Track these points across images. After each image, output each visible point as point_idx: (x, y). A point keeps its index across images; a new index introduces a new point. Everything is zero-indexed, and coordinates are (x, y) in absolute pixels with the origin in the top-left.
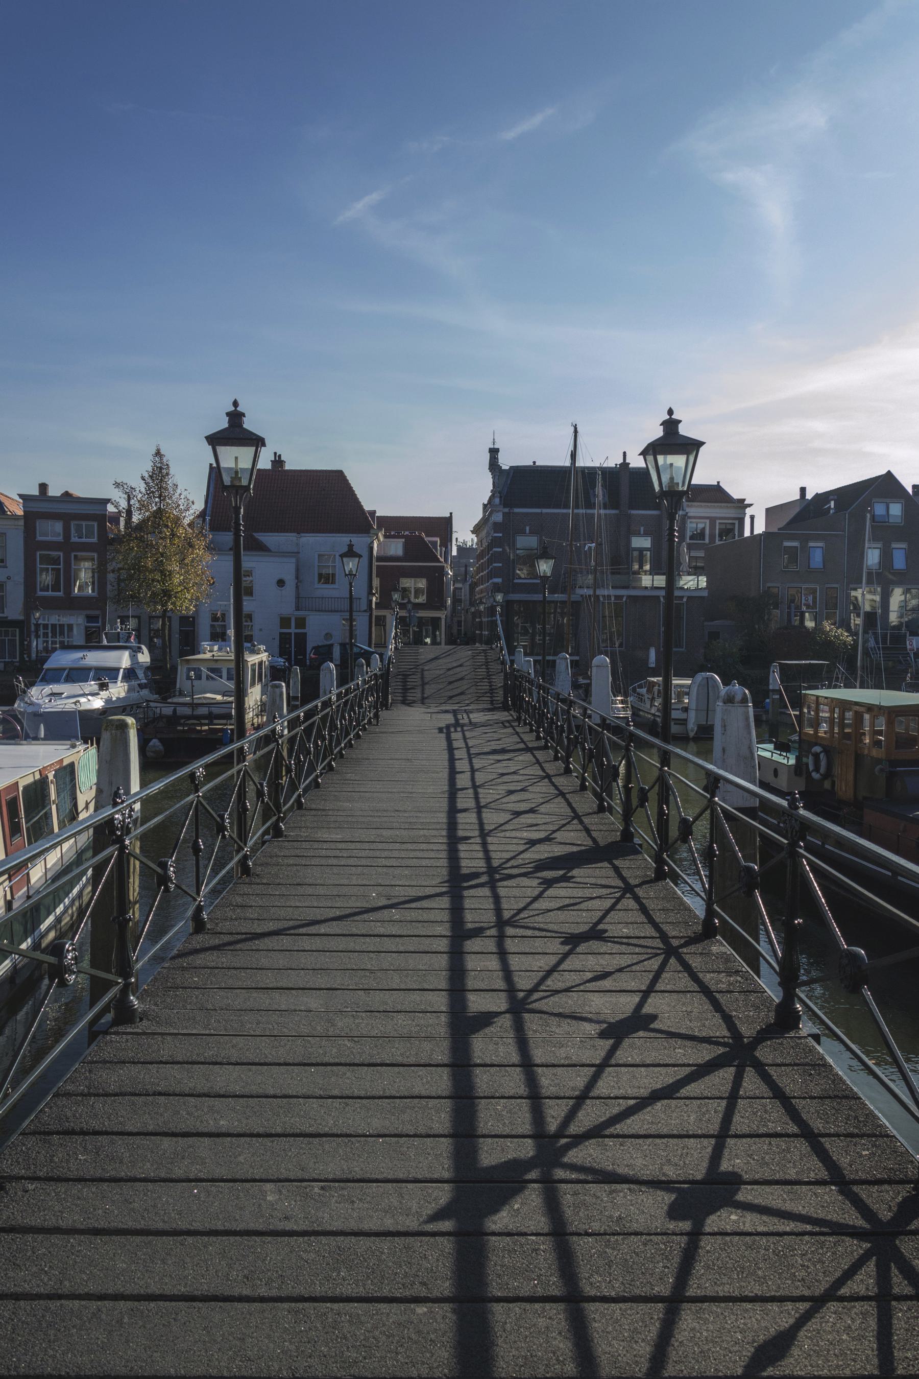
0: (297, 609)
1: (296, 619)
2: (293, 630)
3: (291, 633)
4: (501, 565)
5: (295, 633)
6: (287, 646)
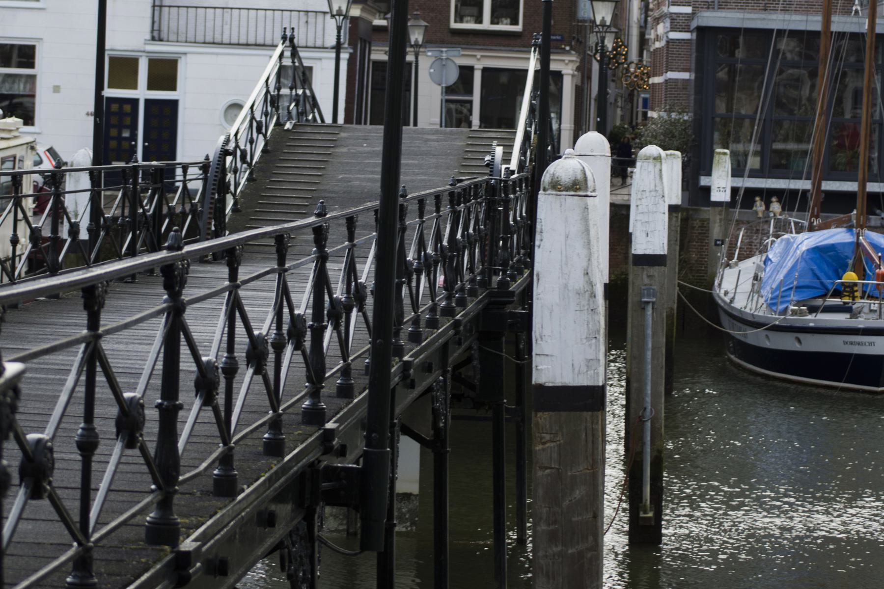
0: (157, 36)
1: (154, 64)
2: (142, 93)
3: (134, 102)
5: (148, 102)
6: (126, 134)
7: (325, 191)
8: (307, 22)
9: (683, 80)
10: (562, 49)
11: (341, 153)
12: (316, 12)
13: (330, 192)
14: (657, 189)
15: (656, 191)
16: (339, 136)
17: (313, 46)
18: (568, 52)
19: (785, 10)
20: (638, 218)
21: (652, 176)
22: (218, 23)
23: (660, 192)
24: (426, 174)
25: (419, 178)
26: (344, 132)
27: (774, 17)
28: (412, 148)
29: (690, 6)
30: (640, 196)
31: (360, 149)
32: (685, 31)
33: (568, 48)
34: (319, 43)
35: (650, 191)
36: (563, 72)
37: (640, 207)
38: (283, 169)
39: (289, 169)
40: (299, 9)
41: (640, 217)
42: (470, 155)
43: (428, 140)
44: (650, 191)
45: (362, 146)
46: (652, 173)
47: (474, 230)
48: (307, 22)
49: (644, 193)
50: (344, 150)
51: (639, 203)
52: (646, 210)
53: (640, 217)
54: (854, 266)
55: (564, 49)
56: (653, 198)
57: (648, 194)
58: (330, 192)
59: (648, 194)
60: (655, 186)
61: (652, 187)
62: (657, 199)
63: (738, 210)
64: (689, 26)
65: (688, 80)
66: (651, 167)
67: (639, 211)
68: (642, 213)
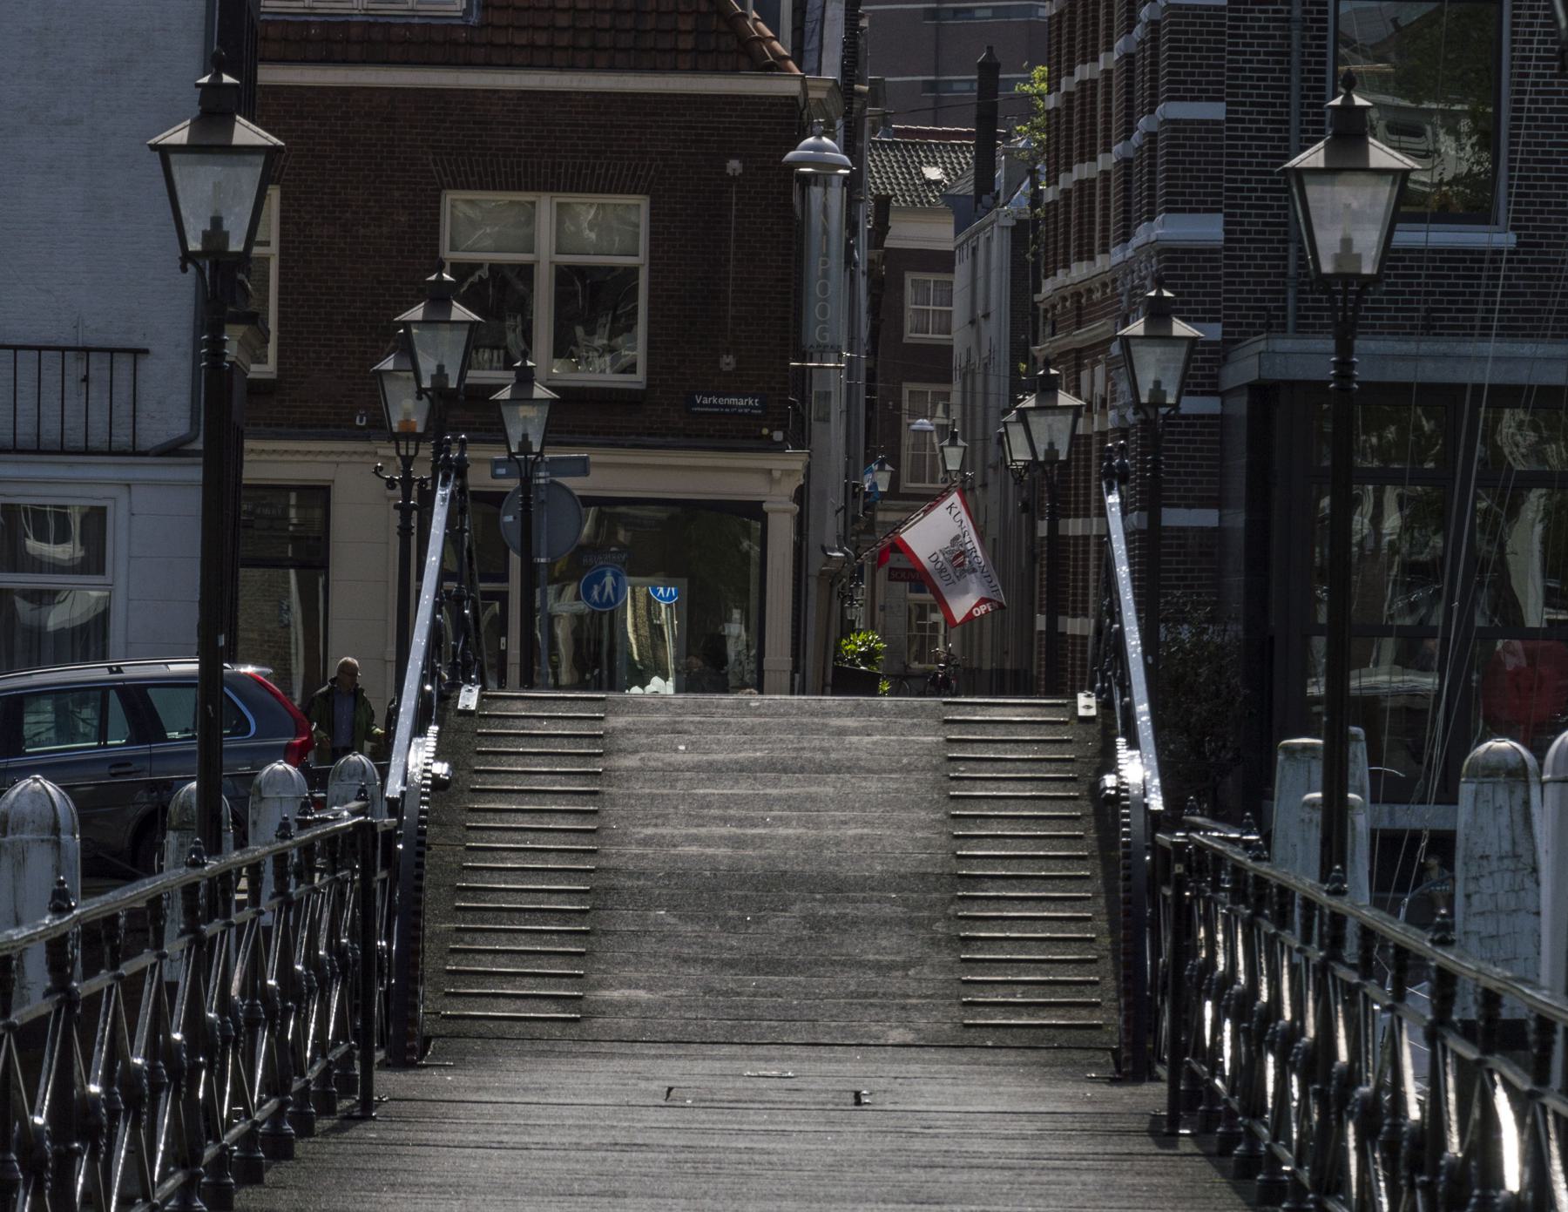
4: (1215, 111)
7: (617, 871)
8: (86, 379)
9: (1202, 529)
10: (761, 437)
11: (627, 769)
12: (112, 351)
13: (630, 875)
14: (1520, 850)
15: (1516, 856)
16: (604, 724)
17: (105, 447)
18: (778, 448)
19: (1510, 331)
20: (1472, 927)
21: (1504, 819)
22: (74, 403)
23: (1527, 859)
24: (866, 823)
25: (851, 832)
26: (616, 714)
27: (1470, 347)
28: (807, 755)
29: (1217, 320)
30: (1474, 871)
31: (669, 757)
32: (1203, 394)
33: (778, 436)
34: (122, 438)
35: (1501, 858)
36: (765, 507)
37: (1475, 899)
38: (489, 816)
39: (505, 816)
40: (62, 343)
41: (1475, 924)
42: (962, 770)
43: (842, 732)
44: (1501, 858)
45: (676, 750)
46: (1506, 810)
47: (329, 948)
48: (86, 379)
49: (1485, 863)
50: (631, 762)
51: (1472, 887)
52: (1491, 906)
53: (1475, 924)
54: (76, 1003)
55: (770, 437)
56: (1508, 876)
57: (1495, 865)
58: (630, 875)
59: (1495, 865)
60: (1514, 843)
61: (1507, 846)
62: (1518, 878)
63: (1391, 895)
64: (1216, 377)
65: (1214, 529)
66: (1502, 796)
67: (1474, 909)
68: (1482, 913)
